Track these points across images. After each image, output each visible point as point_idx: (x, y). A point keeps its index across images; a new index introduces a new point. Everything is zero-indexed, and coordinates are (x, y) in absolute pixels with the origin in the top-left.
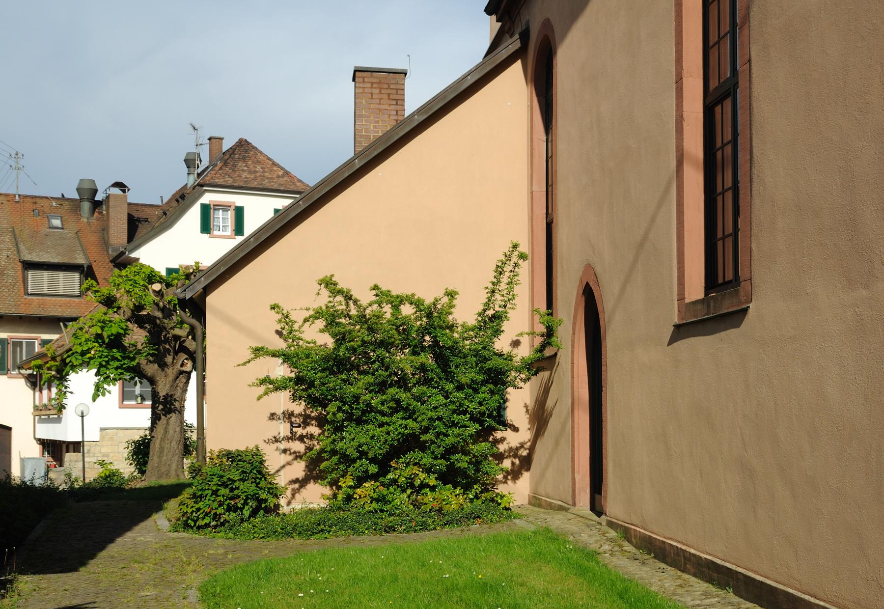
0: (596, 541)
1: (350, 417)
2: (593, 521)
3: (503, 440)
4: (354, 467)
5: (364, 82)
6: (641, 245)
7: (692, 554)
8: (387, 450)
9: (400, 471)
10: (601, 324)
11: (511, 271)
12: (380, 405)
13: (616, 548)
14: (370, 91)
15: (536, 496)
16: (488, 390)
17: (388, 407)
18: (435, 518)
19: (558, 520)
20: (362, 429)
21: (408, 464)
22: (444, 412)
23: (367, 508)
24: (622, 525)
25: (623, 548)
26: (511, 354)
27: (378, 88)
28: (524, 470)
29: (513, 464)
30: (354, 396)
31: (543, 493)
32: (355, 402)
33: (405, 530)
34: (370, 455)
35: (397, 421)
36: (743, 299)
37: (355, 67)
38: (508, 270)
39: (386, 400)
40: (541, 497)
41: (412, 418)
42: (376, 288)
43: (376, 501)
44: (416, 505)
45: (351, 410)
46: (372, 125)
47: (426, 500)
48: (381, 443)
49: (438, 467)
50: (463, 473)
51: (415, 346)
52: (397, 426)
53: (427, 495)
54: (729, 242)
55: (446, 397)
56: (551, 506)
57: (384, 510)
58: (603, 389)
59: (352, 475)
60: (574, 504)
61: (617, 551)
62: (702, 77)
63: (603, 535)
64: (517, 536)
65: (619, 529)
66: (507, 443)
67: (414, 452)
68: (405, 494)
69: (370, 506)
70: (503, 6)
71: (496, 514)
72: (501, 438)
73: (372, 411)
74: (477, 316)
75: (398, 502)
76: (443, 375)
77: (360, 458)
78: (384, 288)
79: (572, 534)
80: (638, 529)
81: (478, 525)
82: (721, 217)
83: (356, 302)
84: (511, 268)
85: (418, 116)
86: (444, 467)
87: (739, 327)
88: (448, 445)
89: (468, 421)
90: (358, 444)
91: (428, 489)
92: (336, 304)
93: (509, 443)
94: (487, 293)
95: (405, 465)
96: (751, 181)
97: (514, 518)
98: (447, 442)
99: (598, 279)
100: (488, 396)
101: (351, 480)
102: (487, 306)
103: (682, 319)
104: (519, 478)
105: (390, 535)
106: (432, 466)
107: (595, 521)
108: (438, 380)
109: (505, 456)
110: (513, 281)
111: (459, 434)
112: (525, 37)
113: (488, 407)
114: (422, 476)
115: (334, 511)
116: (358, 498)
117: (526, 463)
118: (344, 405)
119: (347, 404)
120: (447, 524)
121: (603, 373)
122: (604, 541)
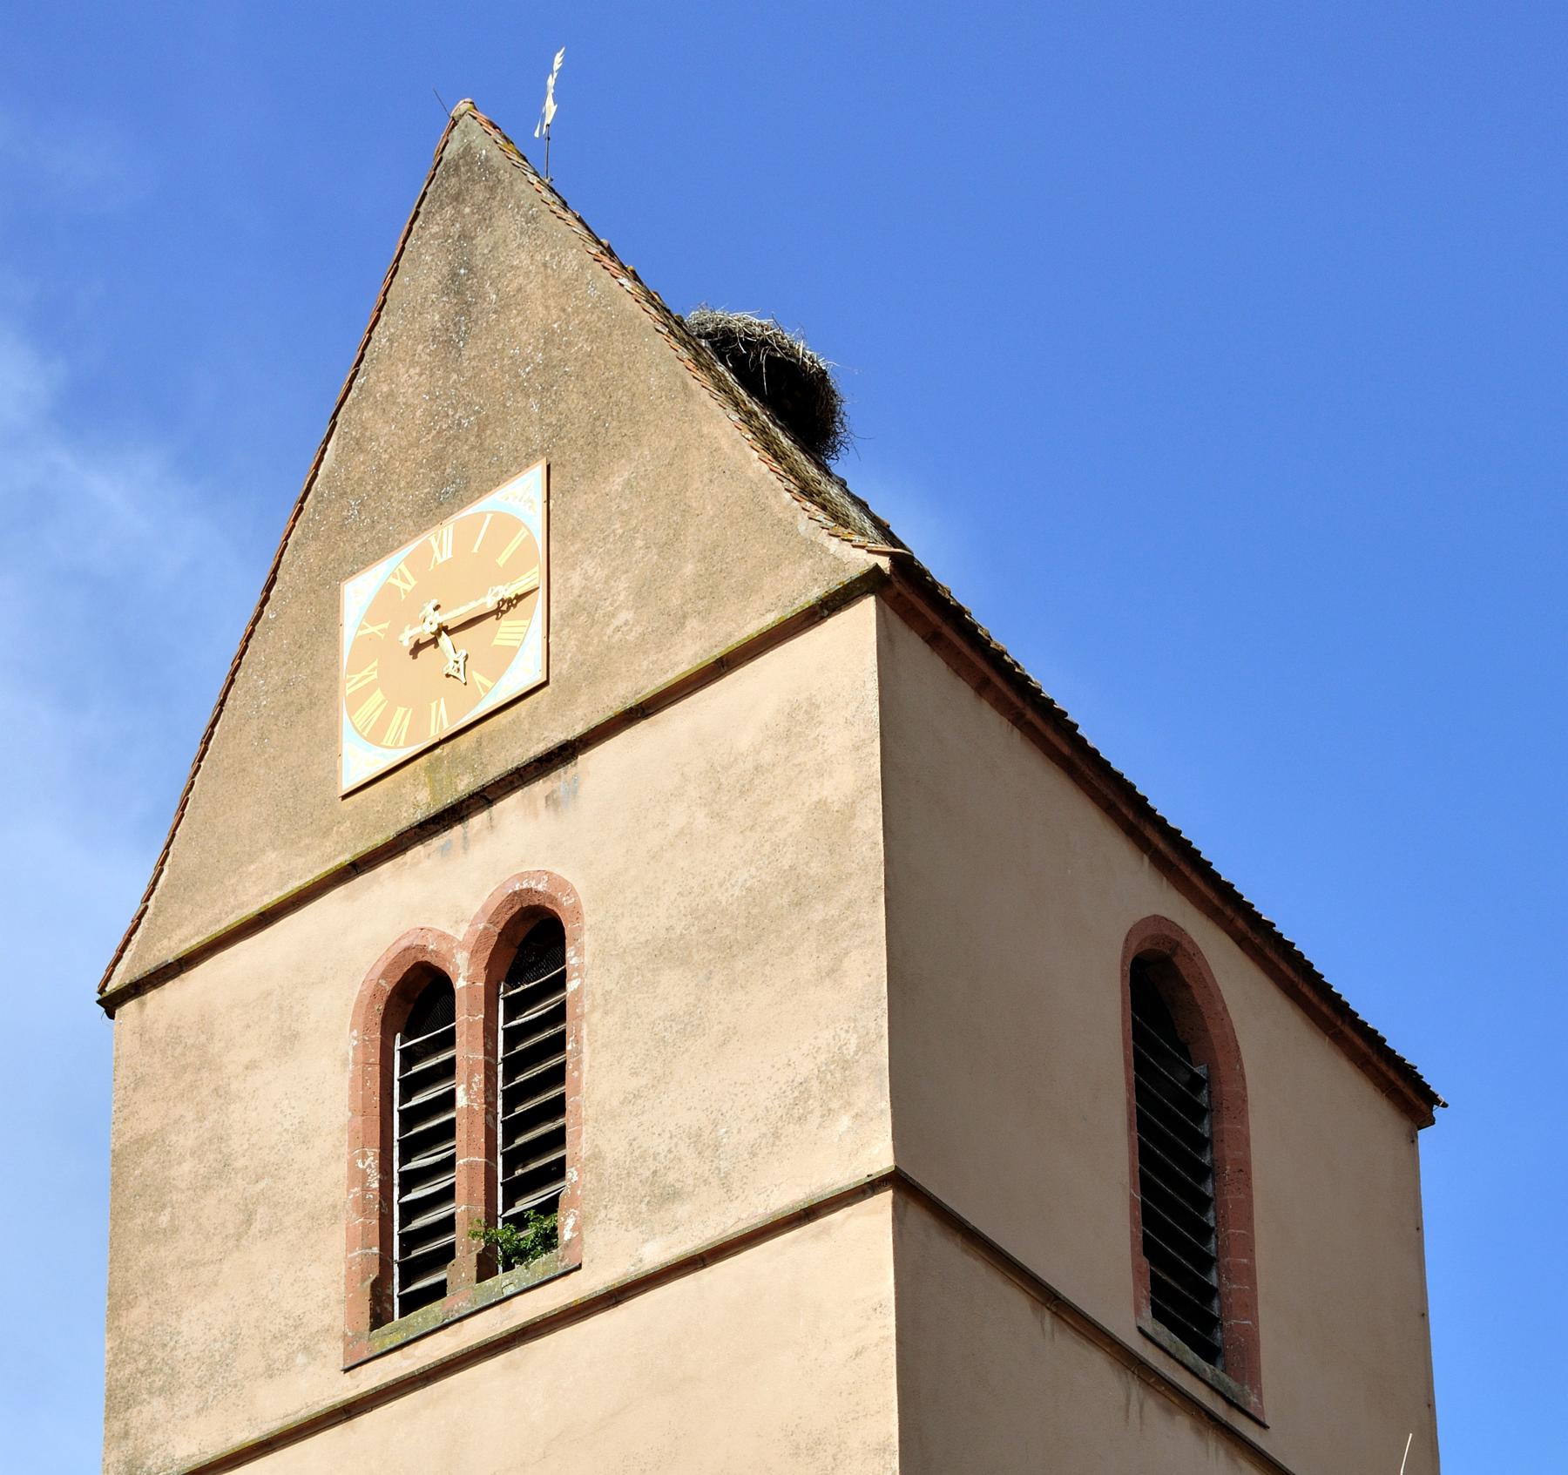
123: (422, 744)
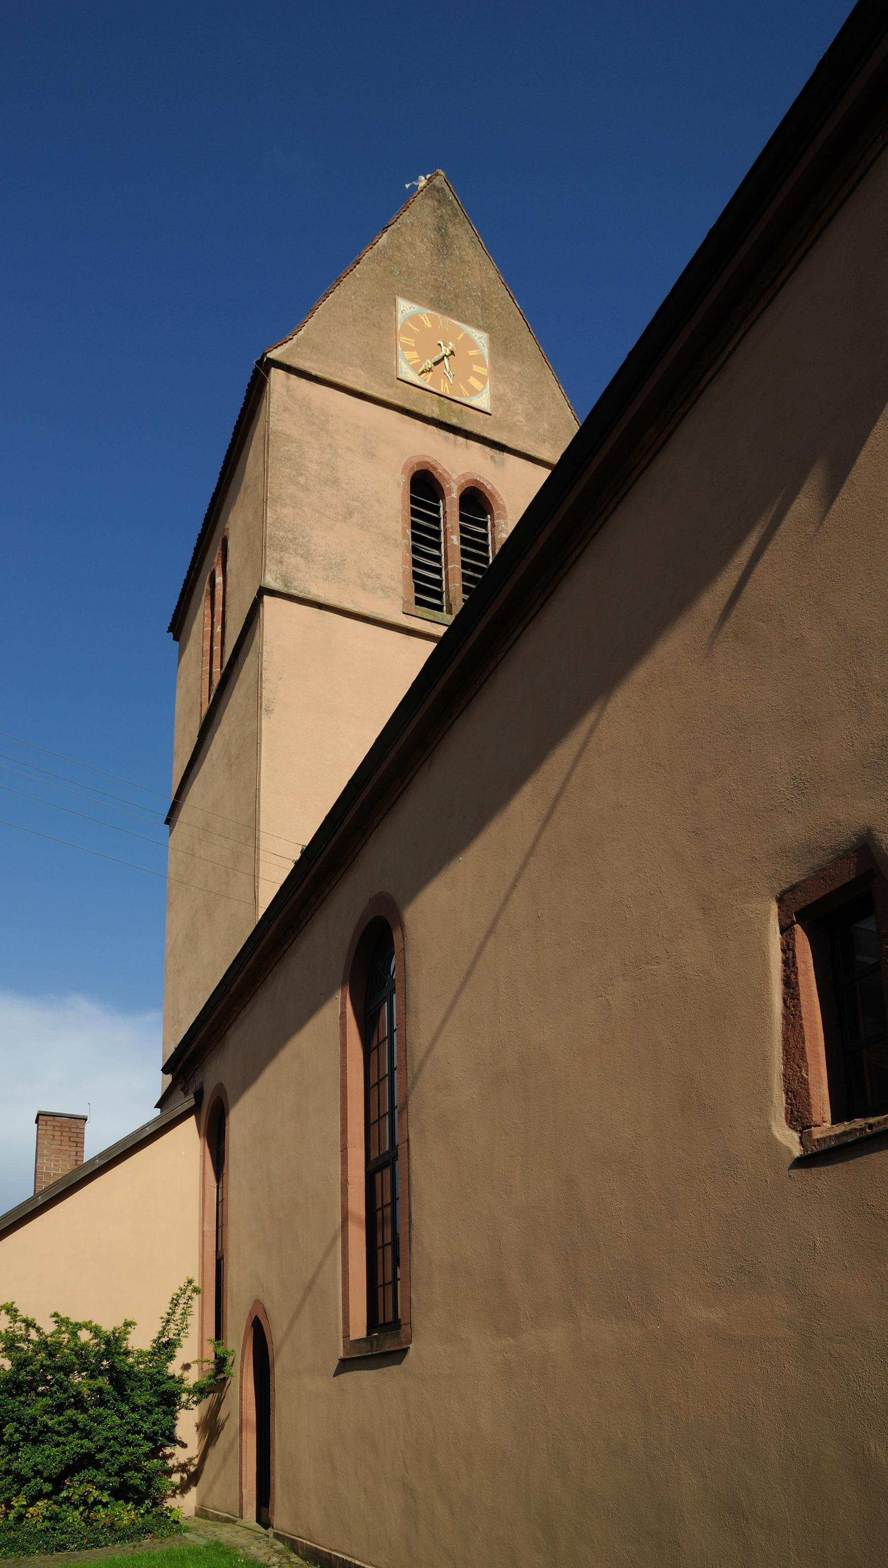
0: (265, 1554)
1: (26, 1438)
2: (260, 1533)
3: (172, 1455)
4: (28, 1486)
5: (46, 1125)
6: (309, 1288)
7: (358, 1565)
8: (62, 1469)
9: (74, 1489)
10: (269, 1353)
11: (185, 1303)
12: (57, 1426)
13: (284, 1560)
14: (51, 1133)
15: (204, 1508)
16: (161, 1411)
17: (65, 1428)
18: (106, 1535)
19: (226, 1532)
20: (38, 1449)
21: (82, 1482)
22: (119, 1432)
23: (38, 1527)
24: (288, 1538)
25: (291, 1560)
26: (183, 1378)
27: (59, 1131)
28: (192, 1485)
29: (182, 1478)
30: (31, 1418)
31: (210, 1505)
32: (32, 1423)
33: (76, 1547)
34: (45, 1475)
35: (73, 1441)
36: (403, 1340)
37: (39, 1111)
38: (183, 1302)
39: (63, 1421)
40: (208, 1509)
41: (88, 1438)
42: (56, 1315)
43: (49, 1519)
44: (88, 1521)
45: (28, 1431)
46: (52, 1163)
47: (98, 1517)
48: (57, 1462)
49: (111, 1484)
50: (135, 1489)
51: (93, 1371)
52: (73, 1445)
53: (99, 1512)
54: (389, 1290)
55: (122, 1418)
56: (217, 1518)
57: (57, 1529)
58: (271, 1411)
59: (25, 1494)
60: (241, 1517)
61: (285, 1563)
62: (364, 1148)
63: (271, 1547)
64: (189, 1552)
65: (286, 1541)
66: (176, 1459)
67: (89, 1470)
68: (78, 1511)
69: (42, 1525)
70: (178, 1068)
71: (167, 1528)
72: (170, 1453)
73: (48, 1431)
74: (152, 1342)
75: (70, 1519)
76: (119, 1398)
77: (34, 1477)
78: (63, 1315)
79: (241, 1547)
80: (305, 1541)
81: (149, 1540)
82: (382, 1266)
83: (38, 1330)
84: (185, 1301)
85: (99, 1160)
86: (117, 1483)
87: (400, 1364)
88: (122, 1463)
89: (142, 1440)
90: (33, 1463)
91: (100, 1506)
92: (16, 1330)
93: (178, 1458)
94: (162, 1322)
95: (79, 1483)
96: (410, 1241)
97: (184, 1532)
98: (121, 1460)
99: (267, 1314)
100: (162, 1417)
101: (24, 1499)
102: (162, 1334)
103: (347, 1354)
104: (187, 1492)
105: (61, 1553)
106: (105, 1483)
107: (263, 1534)
108: (114, 1402)
109: (174, 1471)
110: (187, 1312)
111: (133, 1453)
112: (199, 1096)
113: (161, 1427)
114: (95, 1493)
115: (4, 1531)
116: (30, 1517)
117: (193, 1479)
118: (21, 1426)
119: (24, 1425)
120: (119, 1540)
121: (271, 1397)
122: (272, 1553)
123: (434, 389)
